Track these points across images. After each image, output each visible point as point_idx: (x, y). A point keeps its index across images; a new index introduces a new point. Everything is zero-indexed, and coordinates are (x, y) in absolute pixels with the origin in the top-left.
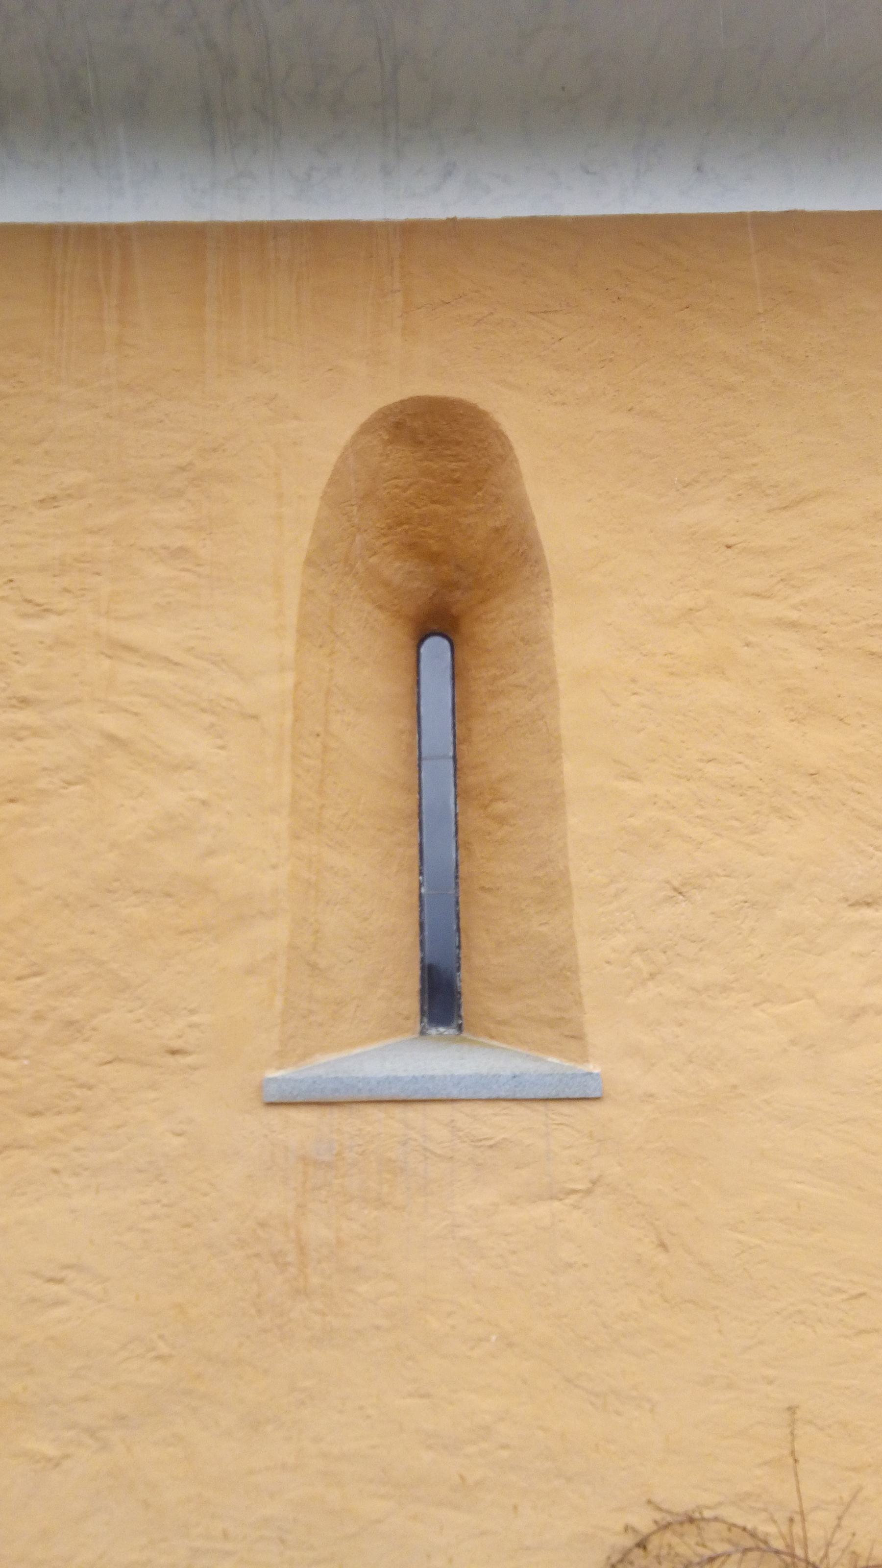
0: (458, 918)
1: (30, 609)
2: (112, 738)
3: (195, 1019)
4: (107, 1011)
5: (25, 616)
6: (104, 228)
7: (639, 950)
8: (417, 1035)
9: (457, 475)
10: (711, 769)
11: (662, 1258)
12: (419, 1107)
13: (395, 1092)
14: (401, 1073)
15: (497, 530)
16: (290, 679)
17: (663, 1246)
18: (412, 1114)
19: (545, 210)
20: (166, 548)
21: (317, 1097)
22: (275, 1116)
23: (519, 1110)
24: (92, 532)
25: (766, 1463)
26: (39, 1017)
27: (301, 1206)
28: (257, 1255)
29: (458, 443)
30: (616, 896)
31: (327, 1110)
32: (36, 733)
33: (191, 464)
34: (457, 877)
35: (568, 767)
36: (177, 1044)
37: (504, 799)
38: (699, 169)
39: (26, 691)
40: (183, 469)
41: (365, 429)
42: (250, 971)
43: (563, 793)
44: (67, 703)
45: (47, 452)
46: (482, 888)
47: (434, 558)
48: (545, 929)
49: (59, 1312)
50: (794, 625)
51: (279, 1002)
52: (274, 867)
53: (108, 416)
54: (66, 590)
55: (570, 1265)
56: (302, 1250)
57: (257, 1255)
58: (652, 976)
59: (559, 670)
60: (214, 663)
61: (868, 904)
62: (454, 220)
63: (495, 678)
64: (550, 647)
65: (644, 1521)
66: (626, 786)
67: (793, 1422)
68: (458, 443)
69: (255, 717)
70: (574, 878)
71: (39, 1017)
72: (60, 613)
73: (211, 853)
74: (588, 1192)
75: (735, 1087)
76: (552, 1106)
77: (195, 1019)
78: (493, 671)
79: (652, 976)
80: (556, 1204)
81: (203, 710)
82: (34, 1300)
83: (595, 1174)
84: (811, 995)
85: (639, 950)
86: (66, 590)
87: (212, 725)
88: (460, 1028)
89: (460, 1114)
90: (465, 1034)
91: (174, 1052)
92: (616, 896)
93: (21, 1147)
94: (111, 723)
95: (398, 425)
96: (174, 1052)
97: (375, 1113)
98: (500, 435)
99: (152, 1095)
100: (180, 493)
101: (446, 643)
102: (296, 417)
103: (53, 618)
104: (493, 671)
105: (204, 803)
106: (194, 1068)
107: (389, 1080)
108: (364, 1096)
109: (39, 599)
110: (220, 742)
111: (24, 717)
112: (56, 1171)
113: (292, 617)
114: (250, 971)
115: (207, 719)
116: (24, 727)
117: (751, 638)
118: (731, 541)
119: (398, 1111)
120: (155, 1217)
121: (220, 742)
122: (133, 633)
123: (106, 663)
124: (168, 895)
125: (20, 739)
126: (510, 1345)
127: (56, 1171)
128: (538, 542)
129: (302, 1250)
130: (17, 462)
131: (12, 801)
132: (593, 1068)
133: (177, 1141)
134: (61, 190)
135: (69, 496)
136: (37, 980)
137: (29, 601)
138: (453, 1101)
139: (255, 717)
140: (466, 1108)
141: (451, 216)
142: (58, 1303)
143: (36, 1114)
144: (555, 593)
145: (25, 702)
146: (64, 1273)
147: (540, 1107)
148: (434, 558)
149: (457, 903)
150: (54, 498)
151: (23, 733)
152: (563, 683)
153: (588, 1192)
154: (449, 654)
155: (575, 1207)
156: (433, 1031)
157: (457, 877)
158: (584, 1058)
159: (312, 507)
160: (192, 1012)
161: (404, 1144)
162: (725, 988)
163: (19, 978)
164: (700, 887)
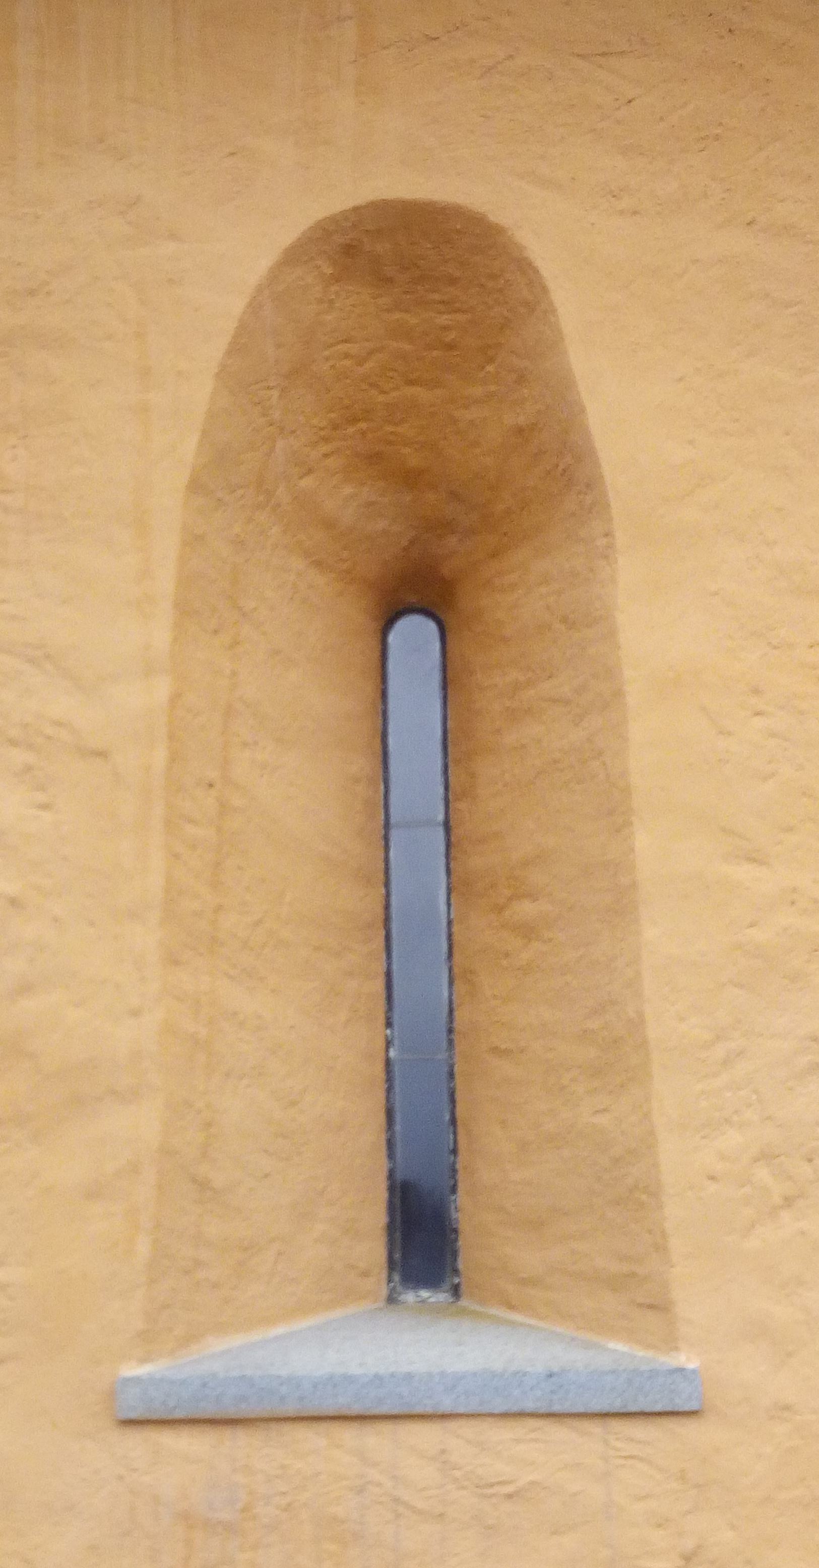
0: (453, 1101)
7: (766, 1156)
8: (381, 1303)
9: (451, 336)
12: (386, 1428)
15: (519, 431)
21: (208, 1409)
29: (453, 281)
30: (726, 1062)
31: (227, 1433)
34: (450, 1031)
37: (532, 896)
43: (634, 885)
48: (603, 1120)
52: (135, 1013)
58: (788, 1201)
60: (31, 661)
66: (743, 872)
68: (453, 281)
69: (102, 754)
70: (653, 1032)
76: (616, 1425)
79: (788, 1201)
81: (13, 743)
83: (689, 1544)
85: (766, 1156)
87: (28, 768)
88: (456, 1291)
90: (464, 1302)
92: (726, 1062)
95: (349, 250)
98: (525, 267)
101: (431, 627)
102: (173, 236)
108: (290, 1409)
110: (41, 797)
119: (348, 1434)
121: (41, 797)
132: (687, 1360)
138: (445, 1417)
139: (102, 754)
140: (468, 1429)
147: (595, 1428)
149: (451, 1075)
152: (634, 695)
154: (437, 645)
156: (410, 1297)
158: (671, 1343)
161: (360, 1491)
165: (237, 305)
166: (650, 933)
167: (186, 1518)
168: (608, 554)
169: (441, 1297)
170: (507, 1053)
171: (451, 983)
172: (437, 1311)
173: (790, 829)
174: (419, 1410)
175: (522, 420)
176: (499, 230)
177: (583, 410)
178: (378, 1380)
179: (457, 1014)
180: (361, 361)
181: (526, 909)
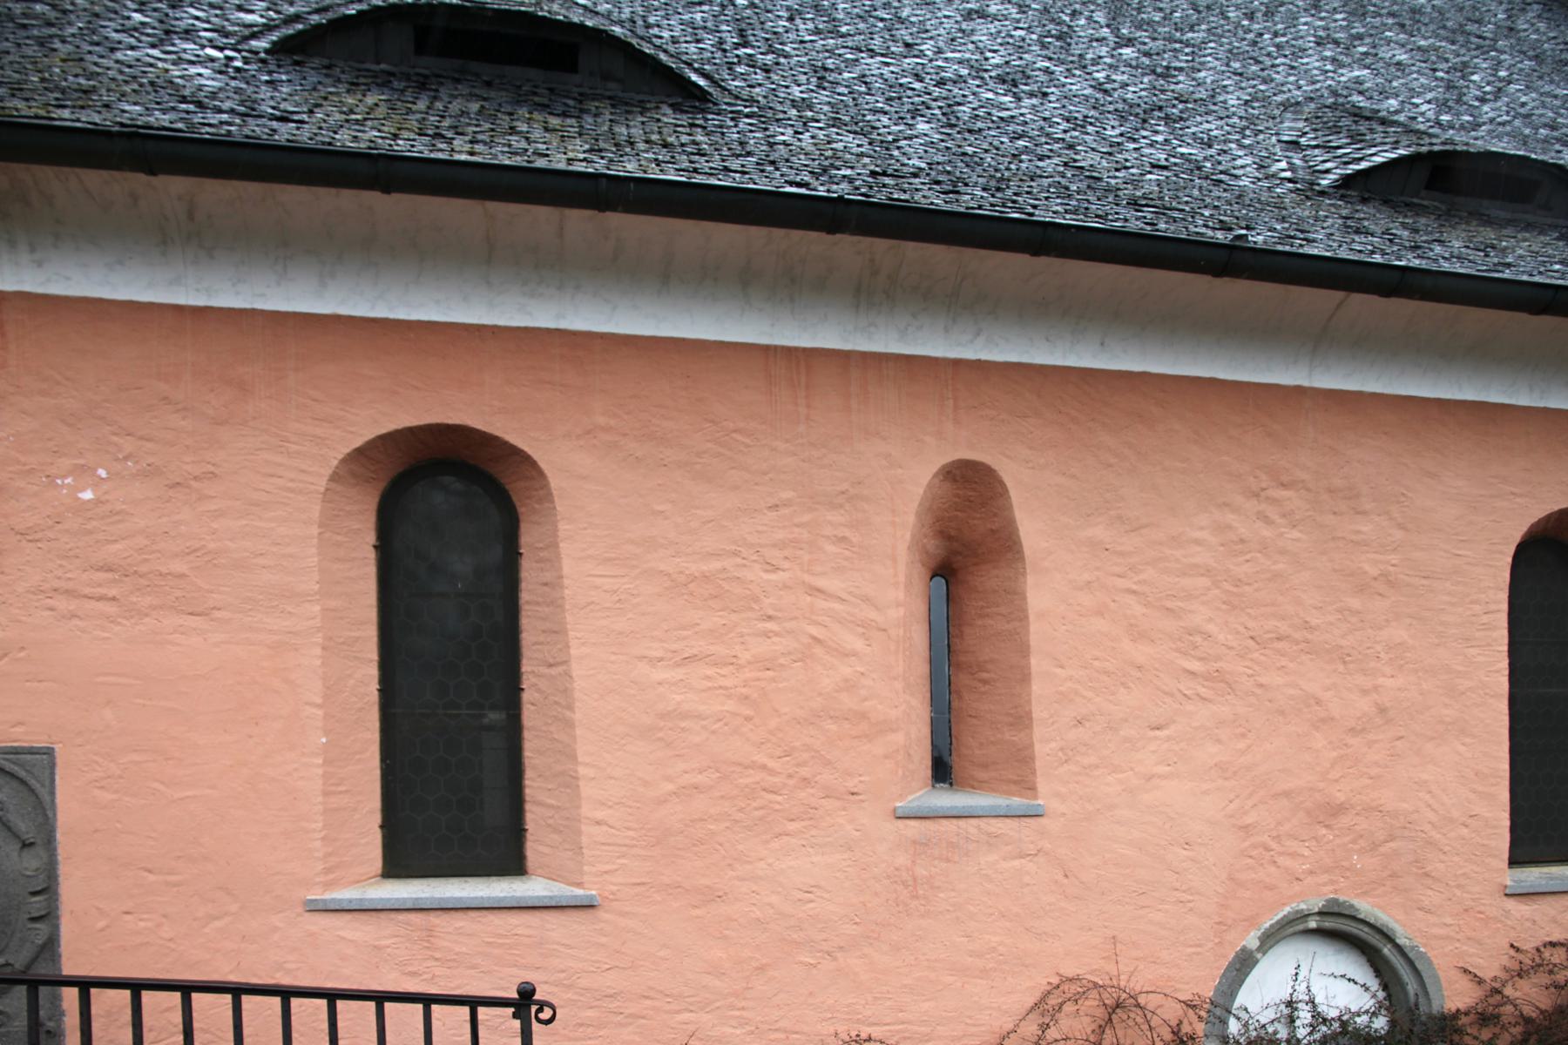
0: (950, 729)
1: (769, 568)
2: (814, 638)
3: (862, 779)
4: (820, 774)
5: (767, 571)
6: (796, 349)
7: (1062, 749)
8: (930, 787)
9: (972, 499)
10: (1096, 663)
11: (1066, 881)
12: (964, 820)
13: (954, 813)
14: (958, 805)
15: (992, 530)
16: (902, 611)
17: (1066, 876)
18: (962, 823)
19: (1025, 359)
20: (835, 536)
21: (919, 815)
22: (900, 823)
23: (1008, 821)
24: (797, 526)
25: (1104, 958)
26: (790, 776)
27: (913, 862)
28: (896, 882)
29: (976, 483)
30: (1053, 723)
31: (923, 821)
32: (777, 634)
33: (847, 490)
34: (950, 708)
35: (1033, 661)
36: (855, 790)
37: (988, 672)
38: (1102, 344)
39: (771, 612)
40: (843, 493)
41: (936, 475)
42: (886, 757)
43: (1030, 673)
44: (791, 619)
45: (771, 480)
46: (970, 716)
47: (950, 538)
48: (1014, 738)
49: (811, 905)
50: (1134, 592)
51: (900, 772)
52: (896, 707)
53: (803, 461)
54: (786, 558)
55: (1028, 885)
56: (915, 880)
57: (896, 882)
58: (1066, 761)
59: (1030, 611)
60: (862, 600)
61: (1158, 729)
62: (979, 360)
63: (982, 607)
64: (1024, 598)
65: (1055, 981)
66: (1059, 671)
67: (1115, 944)
68: (976, 483)
69: (885, 630)
70: (1034, 715)
71: (790, 776)
72: (783, 570)
73: (866, 699)
74: (1036, 855)
75: (1098, 810)
76: (1022, 819)
77: (862, 779)
78: (981, 603)
79: (1066, 761)
80: (1023, 860)
81: (858, 625)
82: (800, 900)
83: (1039, 847)
84: (1132, 769)
85: (1062, 749)
86: (786, 558)
87: (864, 633)
88: (951, 784)
89: (982, 823)
90: (954, 787)
91: (853, 794)
92: (1053, 723)
93: (787, 835)
94: (814, 630)
95: (948, 472)
96: (853, 794)
97: (944, 822)
98: (1002, 483)
99: (844, 813)
100: (841, 506)
101: (943, 581)
102: (900, 467)
103: (781, 573)
104: (981, 603)
105: (862, 674)
106: (863, 801)
107: (433, 899)
108: (941, 814)
109: (774, 563)
110: (867, 643)
111: (770, 625)
112: (804, 846)
113: (902, 578)
114: (886, 757)
115: (861, 630)
116: (771, 631)
117: (1116, 598)
118: (1108, 547)
119: (954, 821)
120: (849, 866)
121: (867, 643)
122: (821, 582)
123: (809, 599)
124: (847, 719)
125: (769, 638)
126: (1003, 916)
127: (804, 846)
128: (1020, 542)
129: (915, 880)
130: (756, 484)
131: (768, 669)
132: (1040, 802)
133: (858, 833)
134: (773, 325)
135: (785, 505)
136: (788, 758)
137: (768, 563)
138: (979, 817)
139: (885, 630)
140: (985, 820)
141: (978, 358)
142: (812, 901)
143: (793, 820)
144: (1028, 571)
145: (770, 618)
146: (811, 889)
147: (1016, 819)
148: (950, 538)
149: (950, 721)
150: (777, 506)
151: (770, 634)
152: (1032, 618)
153: (1036, 855)
154: (945, 588)
155: (1030, 861)
156: (938, 785)
157: (950, 708)
158: (1035, 797)
159: (911, 519)
160: (860, 775)
161: (958, 835)
162: (1097, 767)
163: (780, 757)
164: (1088, 720)
165: (921, 491)
166: (1035, 687)
167: (914, 842)
168: (1024, 574)
169: (947, 786)
170: (975, 717)
171: (950, 693)
172: (946, 789)
173: (1070, 658)
174: (348, 917)
175: (994, 528)
176: (995, 471)
177: (1018, 529)
178: (964, 807)
179: (952, 704)
180: (944, 504)
181: (985, 675)
